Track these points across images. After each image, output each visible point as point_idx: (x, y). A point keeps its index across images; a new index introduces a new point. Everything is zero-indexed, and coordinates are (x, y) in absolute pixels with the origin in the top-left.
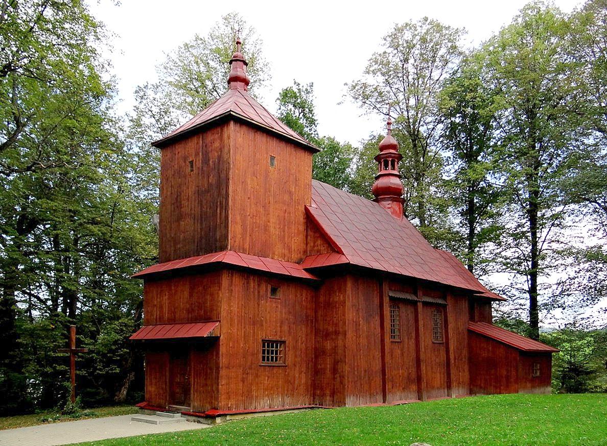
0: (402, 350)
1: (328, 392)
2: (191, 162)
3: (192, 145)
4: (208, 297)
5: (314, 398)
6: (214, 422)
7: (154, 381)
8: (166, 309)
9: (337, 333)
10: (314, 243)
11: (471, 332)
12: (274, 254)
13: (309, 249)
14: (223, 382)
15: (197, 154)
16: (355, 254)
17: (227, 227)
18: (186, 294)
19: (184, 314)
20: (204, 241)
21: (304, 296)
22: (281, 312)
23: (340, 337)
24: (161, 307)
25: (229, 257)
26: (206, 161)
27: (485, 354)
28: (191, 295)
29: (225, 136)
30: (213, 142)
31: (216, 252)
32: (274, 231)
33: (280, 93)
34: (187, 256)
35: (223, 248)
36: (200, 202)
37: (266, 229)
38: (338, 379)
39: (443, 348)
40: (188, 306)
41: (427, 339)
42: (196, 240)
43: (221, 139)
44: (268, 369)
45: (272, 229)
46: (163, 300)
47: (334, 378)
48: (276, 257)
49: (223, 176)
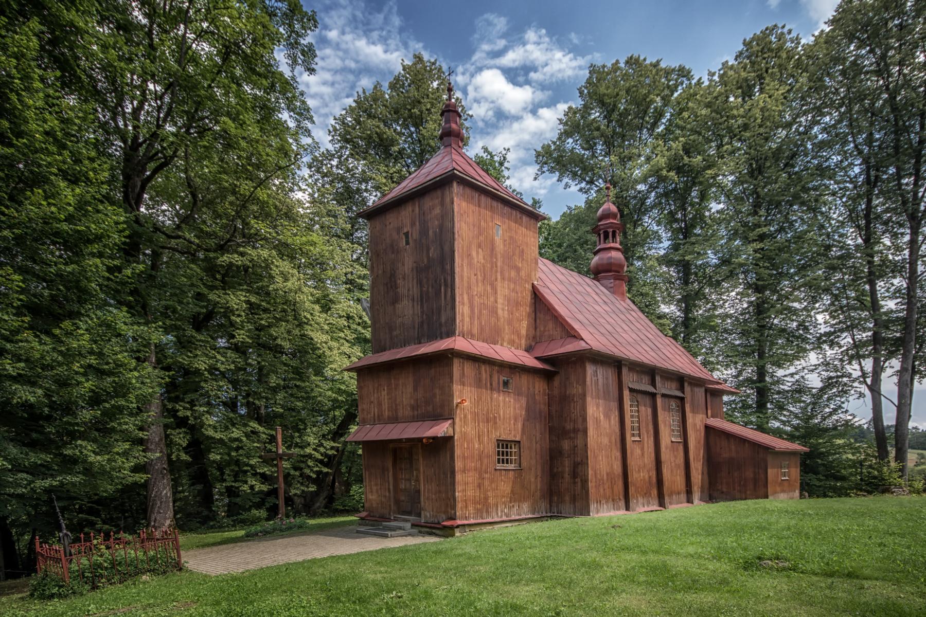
0: (642, 449)
1: (567, 498)
2: (407, 234)
3: (406, 214)
4: (437, 391)
5: (551, 506)
6: (453, 535)
7: (374, 488)
8: (385, 406)
9: (576, 431)
10: (545, 327)
11: (708, 428)
12: (503, 340)
13: (538, 334)
14: (459, 488)
15: (413, 224)
16: (593, 339)
17: (453, 308)
18: (410, 389)
19: (408, 412)
20: (425, 327)
21: (539, 386)
22: (515, 408)
23: (580, 435)
24: (380, 404)
25: (459, 343)
26: (424, 232)
27: (726, 455)
28: (415, 389)
29: (448, 200)
30: (432, 209)
31: (442, 338)
32: (503, 313)
33: (560, 120)
34: (405, 343)
35: (450, 333)
36: (420, 283)
37: (494, 311)
38: (579, 484)
39: (681, 447)
40: (412, 402)
41: (668, 437)
42: (417, 326)
43: (442, 204)
44: (503, 472)
45: (500, 312)
46: (381, 396)
47: (575, 483)
48: (505, 344)
49: (446, 248)
